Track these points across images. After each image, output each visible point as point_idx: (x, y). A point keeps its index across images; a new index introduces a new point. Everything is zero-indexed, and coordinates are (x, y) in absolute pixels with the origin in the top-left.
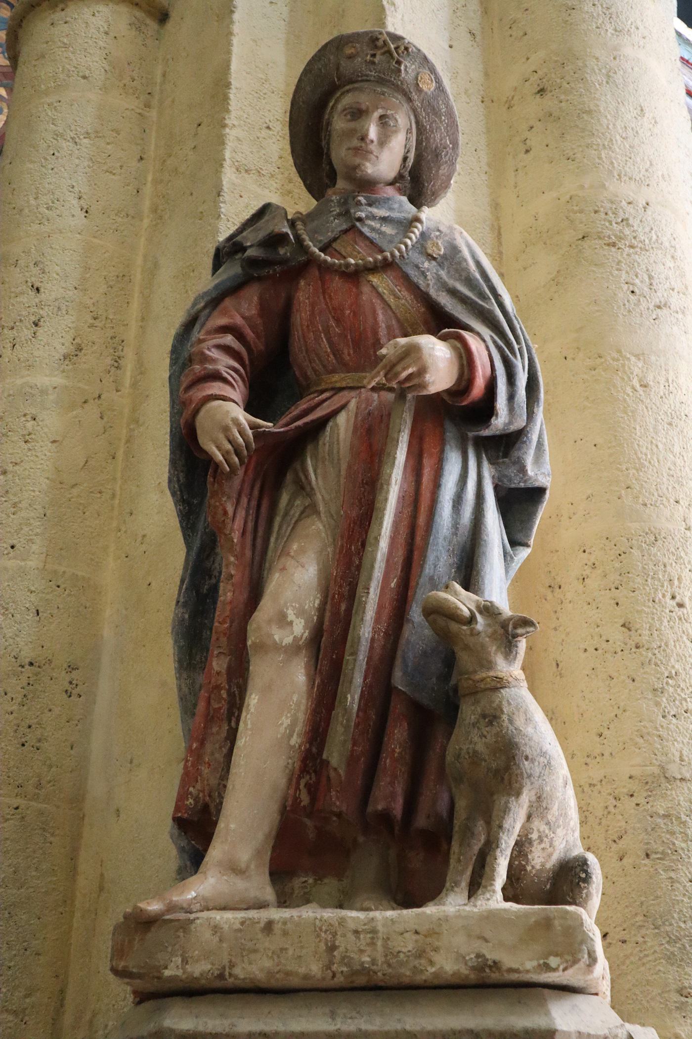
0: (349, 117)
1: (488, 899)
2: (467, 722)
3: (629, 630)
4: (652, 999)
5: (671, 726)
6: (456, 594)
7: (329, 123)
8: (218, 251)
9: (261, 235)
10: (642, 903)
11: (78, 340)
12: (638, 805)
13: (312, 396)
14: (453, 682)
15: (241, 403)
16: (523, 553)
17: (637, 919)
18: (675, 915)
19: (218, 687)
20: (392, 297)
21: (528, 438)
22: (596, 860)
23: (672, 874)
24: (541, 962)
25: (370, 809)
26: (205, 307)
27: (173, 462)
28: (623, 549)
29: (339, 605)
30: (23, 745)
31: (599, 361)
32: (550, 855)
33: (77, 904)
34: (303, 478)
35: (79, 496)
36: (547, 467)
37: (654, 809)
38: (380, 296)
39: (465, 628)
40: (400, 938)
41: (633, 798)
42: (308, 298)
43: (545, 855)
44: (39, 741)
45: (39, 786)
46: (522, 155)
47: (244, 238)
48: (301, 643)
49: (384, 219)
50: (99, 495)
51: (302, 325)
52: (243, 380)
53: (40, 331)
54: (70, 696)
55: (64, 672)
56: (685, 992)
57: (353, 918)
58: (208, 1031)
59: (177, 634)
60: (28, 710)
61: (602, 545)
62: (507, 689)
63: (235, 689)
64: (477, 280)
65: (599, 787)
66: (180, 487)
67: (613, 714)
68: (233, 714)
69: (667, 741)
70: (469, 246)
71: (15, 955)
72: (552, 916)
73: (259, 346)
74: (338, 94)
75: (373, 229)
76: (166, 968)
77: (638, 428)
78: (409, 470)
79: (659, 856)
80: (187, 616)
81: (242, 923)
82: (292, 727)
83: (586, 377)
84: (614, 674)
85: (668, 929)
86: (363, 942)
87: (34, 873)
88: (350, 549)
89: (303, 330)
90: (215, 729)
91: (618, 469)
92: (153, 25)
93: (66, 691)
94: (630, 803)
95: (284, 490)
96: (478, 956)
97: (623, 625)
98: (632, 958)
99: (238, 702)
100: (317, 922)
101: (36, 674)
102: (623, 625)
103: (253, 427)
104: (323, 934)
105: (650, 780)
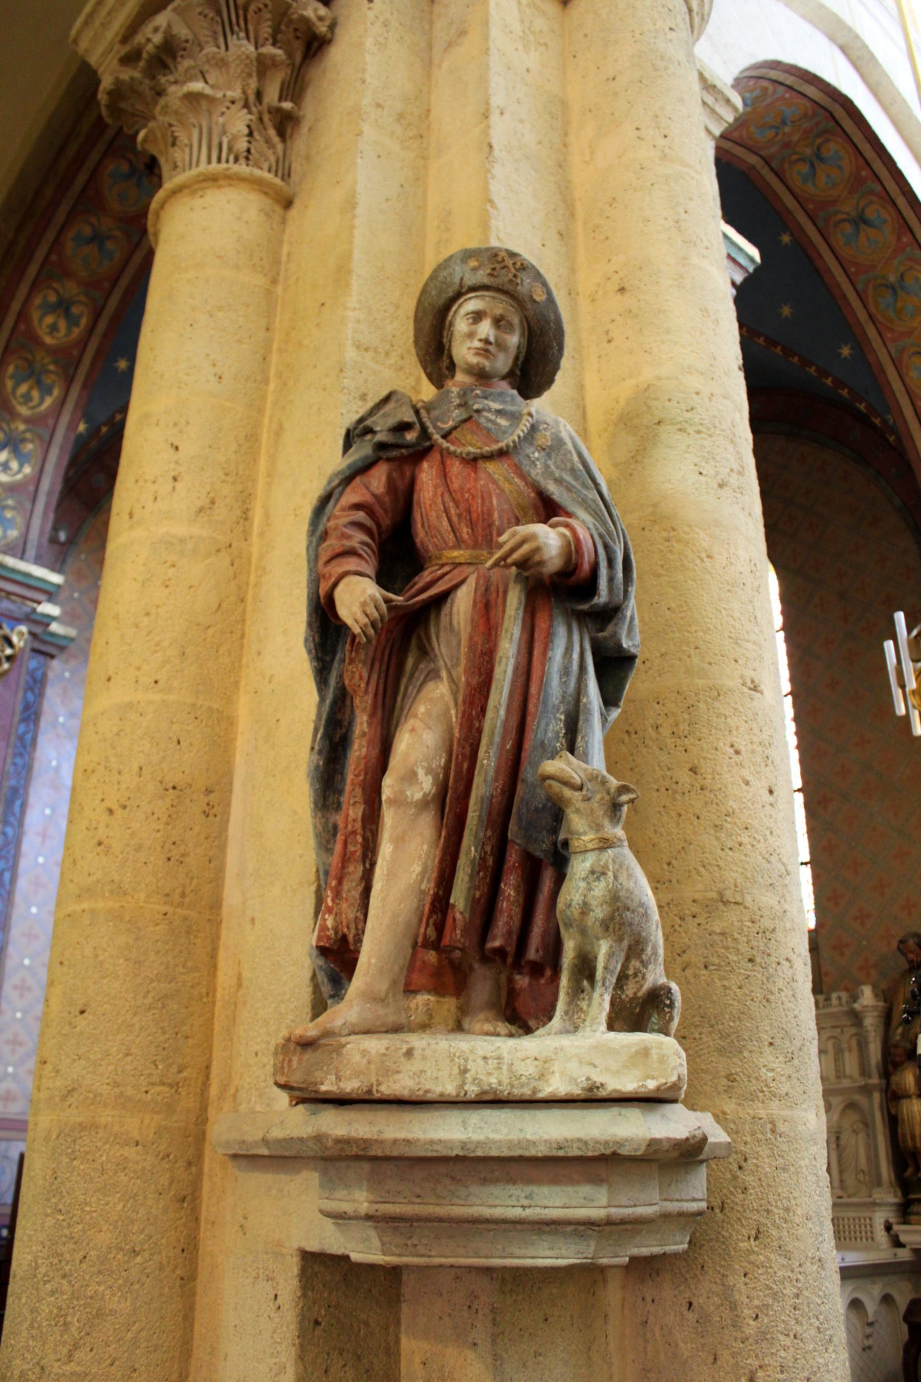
0: (471, 321)
1: (595, 1031)
2: (577, 877)
3: (696, 773)
4: (706, 1084)
5: (729, 859)
7: (451, 324)
8: (348, 434)
9: (392, 421)
10: (700, 1006)
11: (212, 495)
12: (699, 925)
13: (434, 568)
14: (562, 836)
15: (374, 577)
16: (615, 713)
18: (727, 1017)
22: (677, 988)
23: (726, 983)
25: (442, 944)
27: (310, 624)
29: (462, 765)
30: (169, 859)
31: (672, 534)
32: (642, 986)
34: (427, 644)
35: (214, 636)
36: (638, 638)
38: (494, 482)
39: (577, 793)
40: (523, 1064)
41: (695, 919)
42: (431, 480)
43: (638, 986)
44: (182, 856)
45: (183, 895)
47: (375, 423)
48: (429, 798)
51: (425, 504)
52: (373, 551)
53: (179, 485)
54: (208, 816)
58: (360, 1136)
59: (313, 778)
60: (174, 828)
61: (673, 699)
62: (613, 850)
63: (369, 834)
67: (680, 847)
69: (725, 870)
70: (571, 438)
72: (649, 1046)
73: (386, 521)
74: (461, 300)
75: (489, 420)
76: (322, 1084)
79: (714, 967)
80: (321, 763)
81: (387, 1049)
82: (423, 873)
83: (662, 547)
85: (721, 1027)
86: (491, 1066)
89: (426, 508)
90: (351, 868)
92: (279, 209)
94: (691, 924)
96: (588, 1079)
97: (691, 770)
99: (371, 845)
100: (452, 1049)
101: (179, 797)
103: (387, 601)
104: (456, 1059)
105: (709, 903)
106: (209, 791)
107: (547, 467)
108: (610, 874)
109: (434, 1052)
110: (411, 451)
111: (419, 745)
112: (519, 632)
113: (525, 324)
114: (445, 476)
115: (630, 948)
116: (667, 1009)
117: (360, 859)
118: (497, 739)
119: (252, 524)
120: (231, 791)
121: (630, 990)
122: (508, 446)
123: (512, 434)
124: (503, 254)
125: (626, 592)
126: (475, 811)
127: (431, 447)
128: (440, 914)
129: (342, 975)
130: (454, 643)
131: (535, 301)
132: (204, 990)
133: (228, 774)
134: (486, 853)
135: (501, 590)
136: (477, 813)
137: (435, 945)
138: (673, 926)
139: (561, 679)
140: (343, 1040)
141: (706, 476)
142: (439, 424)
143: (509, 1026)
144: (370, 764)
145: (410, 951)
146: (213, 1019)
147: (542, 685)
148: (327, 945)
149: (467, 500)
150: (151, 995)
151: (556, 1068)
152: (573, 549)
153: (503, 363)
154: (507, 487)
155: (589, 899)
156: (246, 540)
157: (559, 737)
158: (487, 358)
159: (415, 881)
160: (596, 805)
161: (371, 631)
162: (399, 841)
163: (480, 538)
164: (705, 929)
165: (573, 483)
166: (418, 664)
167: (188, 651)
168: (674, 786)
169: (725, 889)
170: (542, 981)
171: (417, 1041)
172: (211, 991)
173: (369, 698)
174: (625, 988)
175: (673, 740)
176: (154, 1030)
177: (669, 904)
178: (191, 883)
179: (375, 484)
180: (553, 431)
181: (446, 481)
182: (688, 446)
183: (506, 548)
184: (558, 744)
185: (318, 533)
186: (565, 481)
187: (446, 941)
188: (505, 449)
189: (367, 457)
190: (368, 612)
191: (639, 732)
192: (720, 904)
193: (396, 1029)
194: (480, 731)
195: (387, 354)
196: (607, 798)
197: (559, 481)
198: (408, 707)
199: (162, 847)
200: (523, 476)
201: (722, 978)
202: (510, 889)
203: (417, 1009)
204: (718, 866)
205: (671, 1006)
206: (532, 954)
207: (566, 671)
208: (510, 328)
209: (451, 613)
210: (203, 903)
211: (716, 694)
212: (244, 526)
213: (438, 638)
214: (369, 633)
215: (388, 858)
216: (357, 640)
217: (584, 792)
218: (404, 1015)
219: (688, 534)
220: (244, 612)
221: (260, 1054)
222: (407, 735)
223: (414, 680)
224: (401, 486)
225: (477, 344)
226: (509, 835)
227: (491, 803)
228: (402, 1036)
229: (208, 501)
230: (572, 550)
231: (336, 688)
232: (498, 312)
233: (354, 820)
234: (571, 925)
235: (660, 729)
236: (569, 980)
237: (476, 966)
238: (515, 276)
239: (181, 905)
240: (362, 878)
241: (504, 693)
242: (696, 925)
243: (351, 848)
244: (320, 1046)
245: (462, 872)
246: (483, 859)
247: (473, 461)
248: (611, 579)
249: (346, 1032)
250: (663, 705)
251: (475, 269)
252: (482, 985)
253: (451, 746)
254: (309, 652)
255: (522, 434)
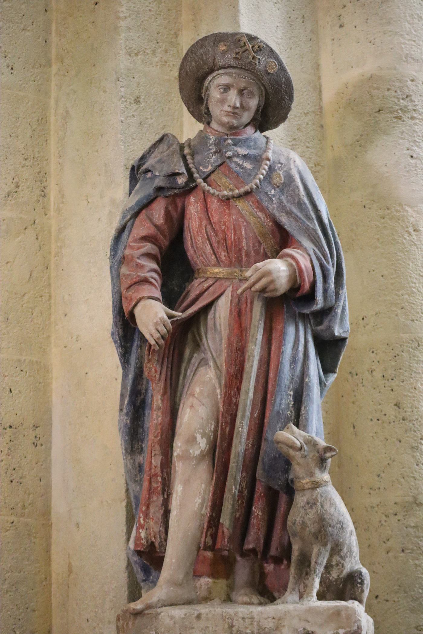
0: (222, 90)
1: (309, 601)
2: (299, 505)
3: (399, 407)
6: (293, 433)
10: (398, 579)
12: (399, 520)
14: (291, 476)
15: (161, 299)
16: (332, 378)
17: (395, 588)
18: (417, 586)
19: (156, 475)
20: (251, 217)
21: (335, 312)
22: (367, 572)
23: (417, 562)
24: (335, 631)
25: (216, 548)
26: (130, 219)
28: (397, 352)
30: (12, 482)
32: (342, 571)
33: (53, 580)
35: (28, 302)
37: (408, 523)
38: (243, 217)
39: (298, 453)
40: (266, 621)
41: (396, 517)
42: (197, 212)
43: (340, 571)
44: (21, 478)
45: (24, 507)
46: (337, 28)
48: (204, 453)
49: (245, 157)
50: (40, 299)
55: (31, 430)
56: (419, 628)
57: (242, 612)
59: (123, 432)
61: (384, 349)
62: (321, 488)
63: (165, 475)
64: (305, 204)
65: (376, 509)
66: (120, 338)
67: (387, 463)
68: (165, 490)
71: (22, 612)
72: (341, 609)
73: (165, 243)
74: (215, 74)
75: (238, 165)
77: (411, 264)
78: (264, 341)
79: (409, 551)
80: (129, 421)
81: (185, 615)
82: (202, 504)
83: (378, 223)
84: (388, 437)
85: (412, 593)
87: (27, 563)
88: (231, 393)
89: (194, 234)
90: (155, 498)
91: (396, 295)
93: (34, 443)
95: (187, 346)
96: (304, 629)
97: (396, 405)
98: (391, 610)
100: (224, 614)
102: (396, 405)
103: (170, 317)
104: (227, 620)
106: (36, 427)
107: (280, 201)
108: (319, 504)
109: (213, 615)
110: (181, 190)
111: (196, 416)
112: (261, 337)
113: (263, 88)
114: (207, 211)
115: (332, 549)
116: (359, 585)
117: (161, 493)
118: (248, 413)
119: (49, 199)
120: (51, 425)
121: (334, 574)
122: (252, 189)
123: (254, 178)
124: (245, 39)
125: (337, 294)
126: (234, 462)
127: (196, 186)
128: (214, 528)
129: (151, 567)
130: (218, 339)
131: (269, 73)
132: (43, 576)
133: (48, 411)
134: (242, 488)
135: (249, 301)
136: (236, 464)
137: (212, 548)
138: (380, 522)
139: (290, 366)
140: (159, 610)
141: (416, 158)
142: (201, 168)
143: (259, 597)
144: (164, 428)
145: (196, 553)
146: (50, 596)
147: (278, 372)
148: (142, 549)
149: (224, 231)
150: (7, 582)
151: (285, 623)
152: (298, 274)
153: (246, 117)
154: (252, 220)
155: (306, 520)
156: (46, 215)
157: (289, 407)
158: (235, 118)
159: (197, 508)
160: (310, 460)
161: (162, 342)
162: (187, 483)
163: (233, 260)
164: (403, 524)
165: (299, 214)
166: (193, 353)
167: (10, 316)
168: (384, 418)
169: (418, 494)
170: (282, 567)
171: (203, 609)
172: (48, 577)
173: (161, 384)
174: (331, 573)
175: (383, 382)
176: (11, 607)
177: (378, 505)
178: (29, 498)
179: (157, 216)
180: (285, 169)
181: (208, 214)
182: (402, 133)
183: (252, 280)
184: (289, 412)
185: (118, 257)
186: (293, 213)
187: (218, 546)
188: (250, 190)
189: (149, 195)
190: (160, 330)
191: (359, 374)
192: (415, 505)
193: (189, 602)
194: (237, 405)
195: (154, 52)
196: (317, 455)
197: (289, 213)
198: (187, 386)
199: (6, 473)
200: (262, 209)
201: (414, 559)
202: (258, 510)
203: (201, 588)
204: (414, 477)
205: (362, 583)
206: (273, 552)
207: (294, 361)
208: (251, 95)
209: (214, 317)
210: (38, 512)
211: (416, 345)
212: (44, 203)
213: (206, 335)
214: (160, 343)
215: (180, 494)
216: (152, 348)
217: (302, 452)
218: (193, 593)
219: (400, 212)
220: (49, 278)
221: (90, 621)
222: (188, 410)
223: (191, 366)
224: (175, 215)
225: (227, 108)
226: (257, 476)
227: (245, 454)
228: (194, 606)
229: (13, 186)
230: (296, 274)
231: (136, 368)
232: (242, 85)
233: (155, 467)
234: (296, 535)
235: (374, 373)
236: (295, 570)
237: (239, 558)
238: (254, 58)
239: (23, 515)
240: (162, 505)
241: (251, 382)
242: (396, 520)
243: (154, 485)
244: (145, 614)
245: (227, 502)
246: (241, 492)
247: (227, 201)
248: (325, 291)
249: (160, 605)
250: (376, 354)
251: (224, 53)
252: (243, 570)
253: (218, 416)
254: (115, 342)
255: (262, 177)
